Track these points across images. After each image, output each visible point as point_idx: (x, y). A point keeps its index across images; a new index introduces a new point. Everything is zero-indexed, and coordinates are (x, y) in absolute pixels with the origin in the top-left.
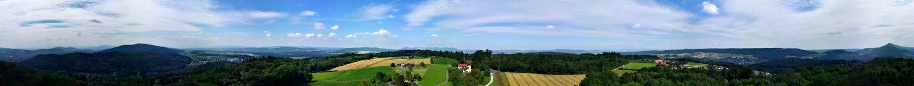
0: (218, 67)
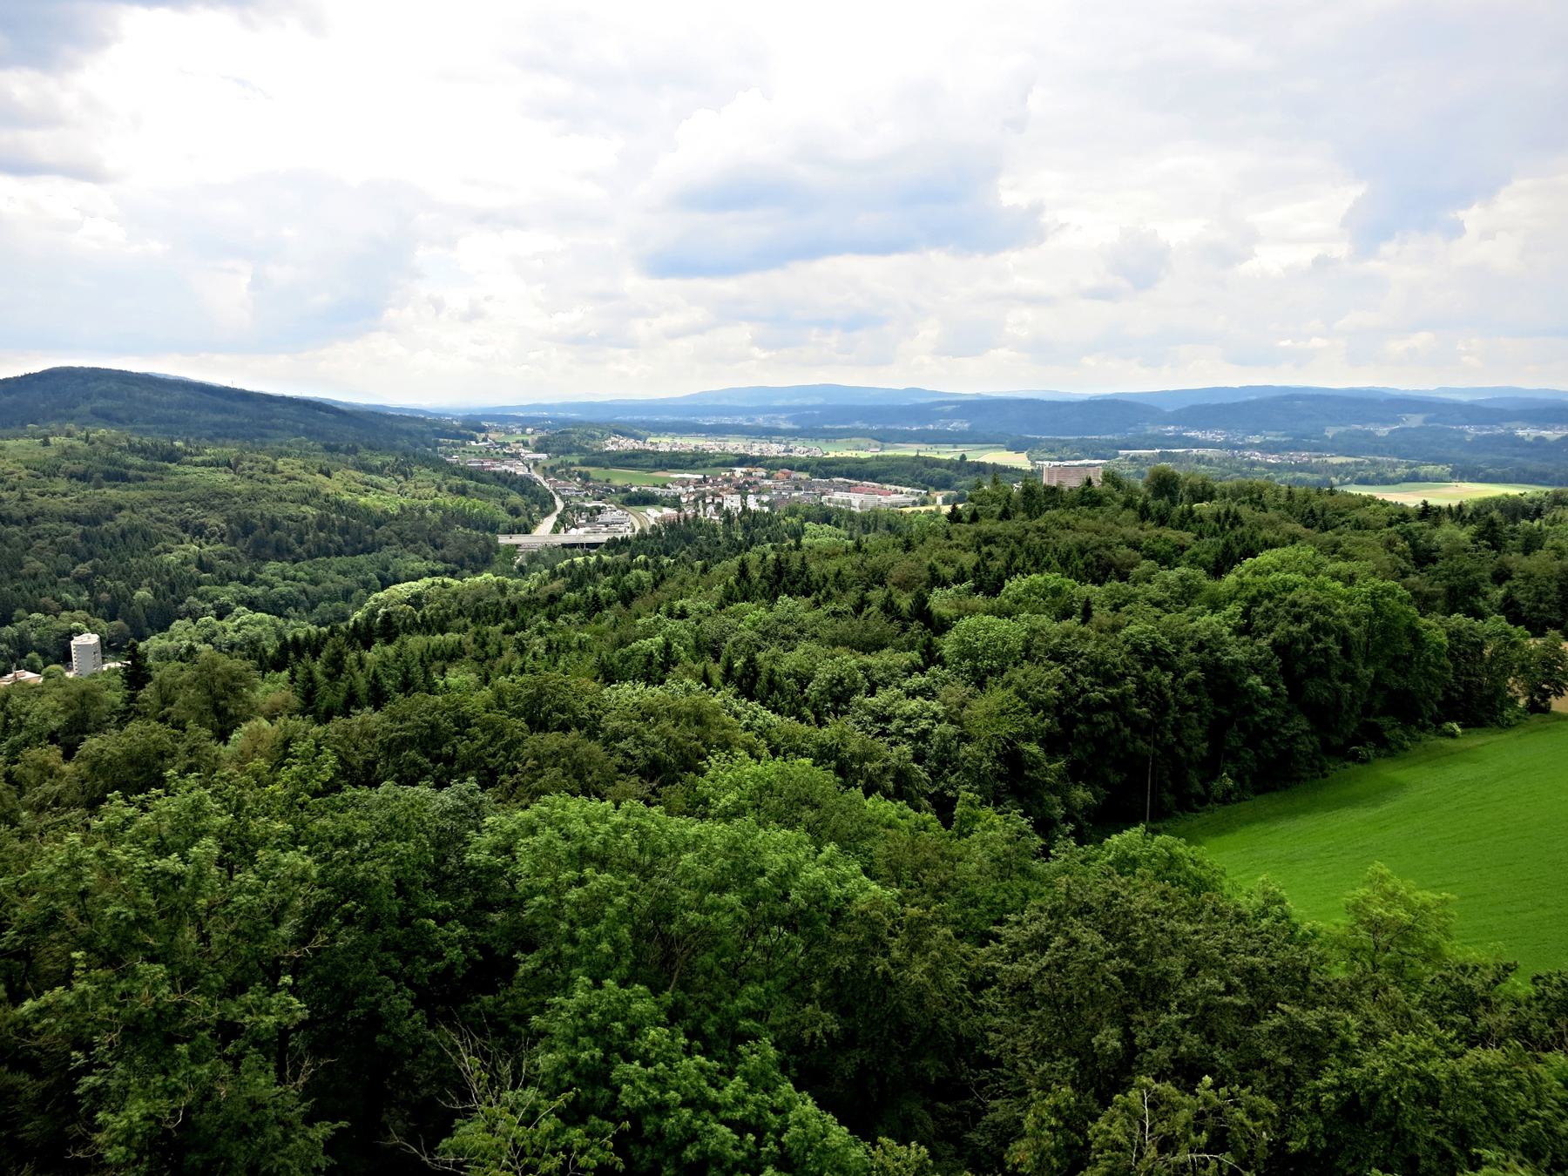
0: (753, 556)
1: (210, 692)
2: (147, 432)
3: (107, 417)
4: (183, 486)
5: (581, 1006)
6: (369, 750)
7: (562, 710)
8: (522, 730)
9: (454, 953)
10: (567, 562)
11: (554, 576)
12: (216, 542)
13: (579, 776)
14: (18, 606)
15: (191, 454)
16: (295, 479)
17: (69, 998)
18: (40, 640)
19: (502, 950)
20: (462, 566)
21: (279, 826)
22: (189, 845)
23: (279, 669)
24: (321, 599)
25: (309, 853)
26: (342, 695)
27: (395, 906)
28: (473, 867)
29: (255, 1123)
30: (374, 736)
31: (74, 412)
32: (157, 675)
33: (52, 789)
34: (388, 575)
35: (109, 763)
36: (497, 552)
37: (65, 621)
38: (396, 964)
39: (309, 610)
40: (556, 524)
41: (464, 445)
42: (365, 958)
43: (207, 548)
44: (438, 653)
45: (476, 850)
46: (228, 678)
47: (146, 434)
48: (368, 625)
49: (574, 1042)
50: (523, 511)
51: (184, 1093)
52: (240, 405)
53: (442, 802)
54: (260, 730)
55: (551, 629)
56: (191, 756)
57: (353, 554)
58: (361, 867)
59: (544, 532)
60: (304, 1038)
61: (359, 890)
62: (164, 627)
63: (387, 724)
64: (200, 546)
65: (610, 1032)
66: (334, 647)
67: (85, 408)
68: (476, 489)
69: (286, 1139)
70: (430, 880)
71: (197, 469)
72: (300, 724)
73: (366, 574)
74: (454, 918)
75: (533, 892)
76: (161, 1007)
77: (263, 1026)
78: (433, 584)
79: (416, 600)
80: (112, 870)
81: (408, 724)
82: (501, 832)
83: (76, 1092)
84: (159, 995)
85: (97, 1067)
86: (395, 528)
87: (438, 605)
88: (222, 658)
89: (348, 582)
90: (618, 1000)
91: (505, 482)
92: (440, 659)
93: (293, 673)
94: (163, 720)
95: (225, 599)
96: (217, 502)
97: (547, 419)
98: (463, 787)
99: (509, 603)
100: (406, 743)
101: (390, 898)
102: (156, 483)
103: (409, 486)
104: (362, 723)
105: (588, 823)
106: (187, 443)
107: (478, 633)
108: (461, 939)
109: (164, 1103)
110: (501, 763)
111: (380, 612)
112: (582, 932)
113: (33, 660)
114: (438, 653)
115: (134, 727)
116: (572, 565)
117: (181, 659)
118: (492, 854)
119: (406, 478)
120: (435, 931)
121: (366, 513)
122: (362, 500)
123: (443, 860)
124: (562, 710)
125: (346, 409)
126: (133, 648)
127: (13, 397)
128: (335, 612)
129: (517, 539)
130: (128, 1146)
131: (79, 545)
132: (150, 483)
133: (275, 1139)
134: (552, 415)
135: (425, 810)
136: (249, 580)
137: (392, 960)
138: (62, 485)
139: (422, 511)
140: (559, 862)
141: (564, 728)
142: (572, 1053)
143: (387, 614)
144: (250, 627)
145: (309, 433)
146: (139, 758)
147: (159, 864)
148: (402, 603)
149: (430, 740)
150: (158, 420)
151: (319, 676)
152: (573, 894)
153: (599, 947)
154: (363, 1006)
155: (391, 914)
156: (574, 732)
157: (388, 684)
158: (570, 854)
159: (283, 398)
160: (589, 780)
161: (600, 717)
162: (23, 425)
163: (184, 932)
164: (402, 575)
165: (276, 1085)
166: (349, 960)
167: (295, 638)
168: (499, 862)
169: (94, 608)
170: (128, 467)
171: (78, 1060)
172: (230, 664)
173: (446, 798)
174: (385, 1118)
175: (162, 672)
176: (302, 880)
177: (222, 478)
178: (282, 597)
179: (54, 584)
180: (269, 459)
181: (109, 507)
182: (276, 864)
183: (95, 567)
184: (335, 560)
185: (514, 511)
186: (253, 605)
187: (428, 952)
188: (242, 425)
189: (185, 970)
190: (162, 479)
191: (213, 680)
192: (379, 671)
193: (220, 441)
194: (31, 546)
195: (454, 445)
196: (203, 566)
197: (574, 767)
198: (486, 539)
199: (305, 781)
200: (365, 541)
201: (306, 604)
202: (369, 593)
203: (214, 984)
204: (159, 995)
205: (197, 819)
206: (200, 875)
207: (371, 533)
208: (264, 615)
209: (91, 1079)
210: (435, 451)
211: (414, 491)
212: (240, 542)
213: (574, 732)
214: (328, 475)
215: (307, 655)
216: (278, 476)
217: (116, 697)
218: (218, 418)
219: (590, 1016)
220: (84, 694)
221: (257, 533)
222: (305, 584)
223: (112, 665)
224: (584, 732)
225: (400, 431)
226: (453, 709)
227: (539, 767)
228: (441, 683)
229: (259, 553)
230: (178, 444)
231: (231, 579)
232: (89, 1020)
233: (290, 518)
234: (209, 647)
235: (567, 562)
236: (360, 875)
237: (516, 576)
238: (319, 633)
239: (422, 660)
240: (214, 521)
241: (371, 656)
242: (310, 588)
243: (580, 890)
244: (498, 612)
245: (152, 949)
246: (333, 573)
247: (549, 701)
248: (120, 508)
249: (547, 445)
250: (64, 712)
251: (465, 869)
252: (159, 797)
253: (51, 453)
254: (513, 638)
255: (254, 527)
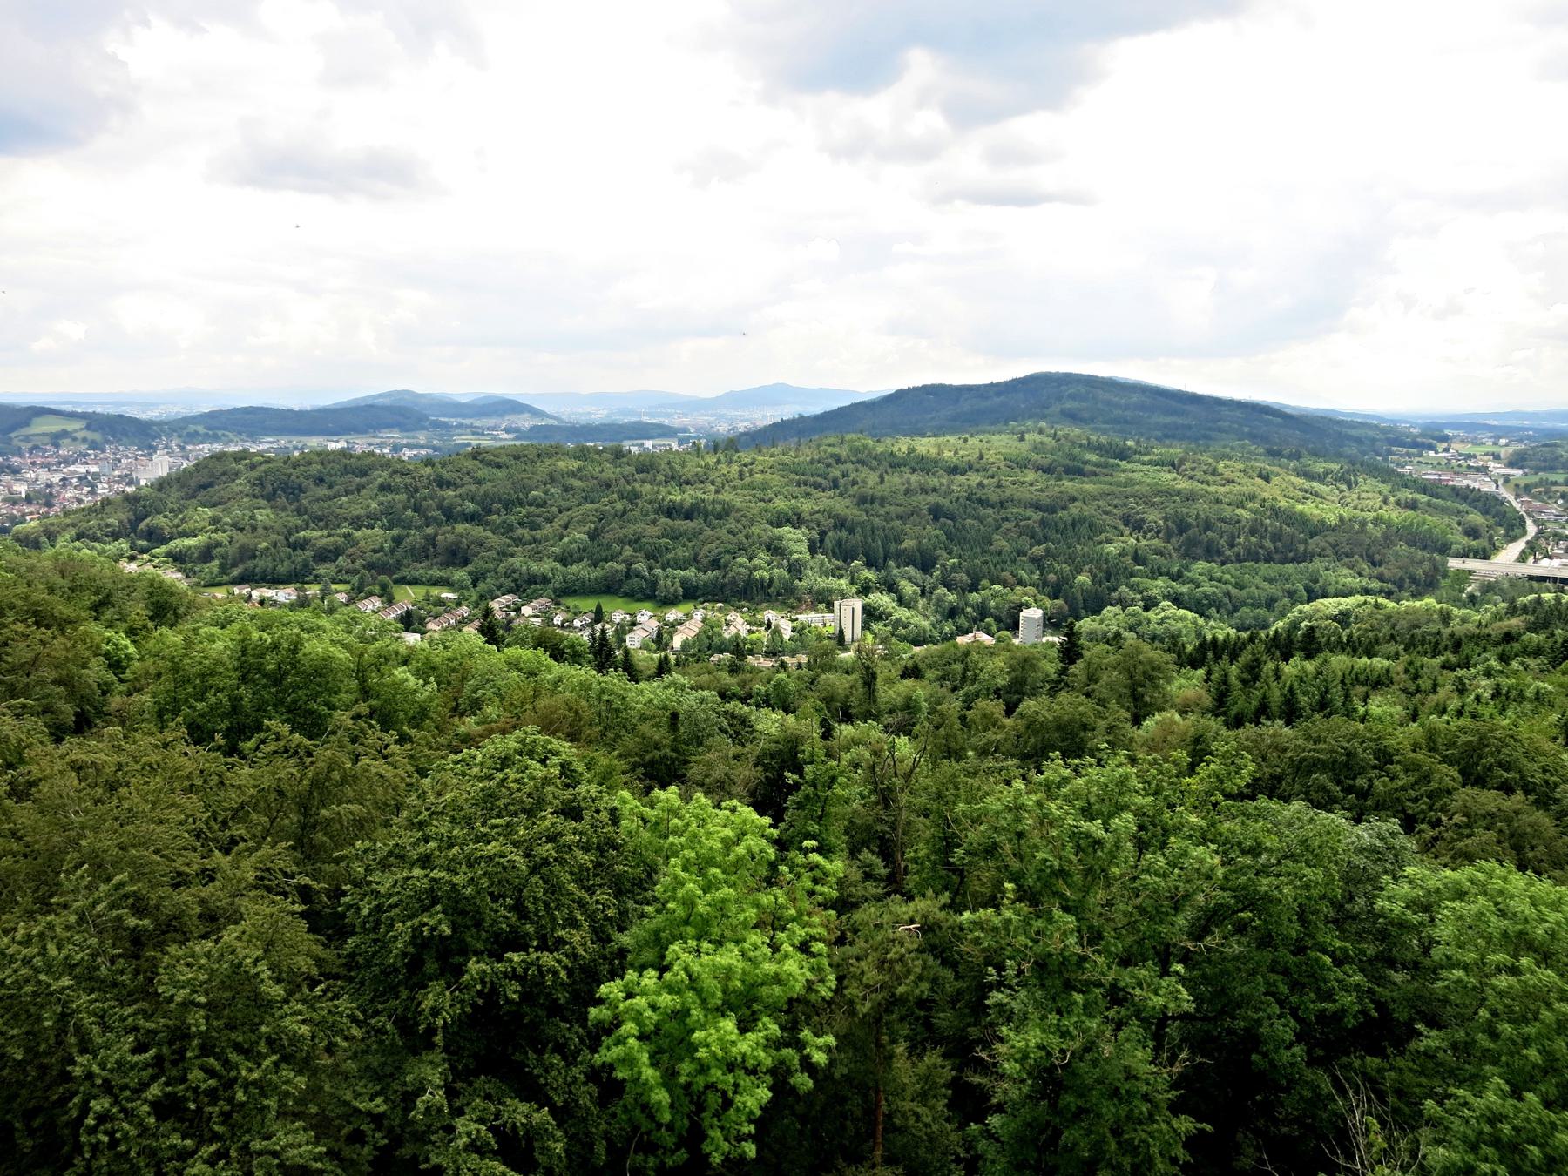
1: (1131, 677)
2: (1105, 432)
3: (1072, 417)
4: (1129, 483)
5: (1490, 1110)
6: (1278, 764)
7: (1507, 767)
8: (1453, 779)
9: (1348, 1000)
10: (1531, 597)
11: (1513, 611)
12: (1153, 538)
13: (1518, 848)
14: (984, 577)
15: (1140, 453)
16: (1233, 482)
17: (997, 921)
18: (997, 608)
19: (1401, 1014)
20: (1401, 588)
21: (1193, 818)
22: (1111, 816)
23: (1195, 667)
24: (1244, 604)
25: (1217, 852)
26: (1255, 703)
27: (1294, 930)
28: (1382, 915)
29: (1127, 1091)
30: (1285, 750)
31: (1046, 412)
32: (1087, 654)
33: (994, 737)
34: (1317, 588)
35: (1042, 724)
36: (1445, 576)
37: (1019, 594)
38: (1284, 989)
39: (1231, 613)
40: (1523, 552)
41: (1420, 455)
42: (1253, 973)
43: (1144, 542)
44: (1362, 678)
45: (1389, 899)
46: (1148, 668)
47: (1104, 434)
48: (1289, 636)
49: (1474, 1148)
50: (1484, 534)
51: (1073, 1038)
52: (1189, 408)
53: (1358, 837)
54: (1173, 722)
55: (1501, 672)
56: (1109, 733)
57: (1283, 562)
58: (1266, 881)
59: (1507, 560)
60: (1180, 1028)
61: (1251, 900)
62: (1097, 611)
63: (1300, 742)
64: (1138, 540)
65: (1523, 1154)
66: (1253, 654)
67: (1056, 408)
68: (1429, 504)
69: (1151, 1119)
70: (1331, 914)
71: (1144, 468)
72: (1214, 724)
73: (1294, 584)
74: (1351, 963)
75: (1451, 963)
76: (1067, 954)
77: (1150, 1004)
78: (1365, 603)
79: (1343, 618)
80: (1045, 820)
81: (1322, 746)
82: (1422, 887)
83: (987, 1002)
84: (1067, 942)
85: (1005, 986)
86: (1331, 540)
87: (1367, 626)
88: (1146, 647)
89: (1273, 590)
90: (1540, 1121)
91: (1465, 499)
92: (1363, 684)
93: (1209, 673)
94: (1088, 695)
95: (1154, 592)
96: (1157, 499)
97: (1527, 429)
98: (1385, 826)
99: (1452, 635)
100: (1316, 765)
101: (1290, 920)
102: (1108, 479)
103: (1352, 497)
104: (1274, 736)
105: (1534, 904)
106: (1138, 442)
107: (1411, 663)
108: (1357, 987)
109: (1056, 1040)
110: (1422, 811)
111: (1303, 625)
112: (1506, 1028)
113: (989, 625)
114: (1362, 678)
115: (1063, 697)
116: (1539, 601)
117: (1108, 643)
118: (1407, 907)
119: (1350, 488)
120: (1329, 969)
121: (1302, 521)
122: (1300, 507)
123: (1351, 898)
124: (1507, 767)
125: (1294, 413)
126: (1071, 626)
127: (1002, 398)
128: (1256, 618)
129: (1471, 564)
130: (1022, 1065)
131: (1038, 530)
132: (1102, 479)
133: (1141, 1113)
134: (1536, 424)
135: (1339, 841)
136: (1177, 577)
137: (1280, 984)
138: (1030, 476)
139: (1363, 524)
140: (1489, 940)
141: (1507, 789)
142: (1470, 1158)
143: (1312, 629)
144: (1173, 622)
145: (1253, 437)
146: (1066, 726)
147: (1085, 826)
148: (1327, 618)
149: (1345, 768)
150: (1116, 421)
151: (1233, 680)
152: (1503, 981)
153: (1525, 1052)
154: (1244, 1019)
155: (1286, 938)
156: (1519, 796)
157: (1304, 701)
158: (1505, 934)
159: (1232, 401)
160: (1530, 855)
161: (1556, 785)
162: (1006, 423)
163: (1097, 893)
164: (1331, 589)
165: (1151, 1063)
166: (1239, 970)
167: (1215, 639)
168: (1414, 918)
169: (1042, 585)
170: (1086, 463)
171: (991, 975)
172: (1152, 654)
173: (1364, 834)
174: (1240, 1137)
175: (1093, 652)
176: (1208, 878)
177: (1167, 477)
178: (1206, 596)
179: (1014, 561)
180: (1210, 461)
181: (1066, 498)
182: (1185, 854)
183: (1047, 550)
184: (1263, 566)
185: (1472, 532)
186: (1177, 601)
187: (1319, 989)
188: (1189, 427)
189: (1091, 928)
190: (1111, 475)
191: (1135, 666)
192: (1296, 686)
193: (1167, 442)
194: (1000, 527)
195: (1408, 455)
196: (1138, 559)
197: (1512, 836)
198: (1432, 560)
199: (1221, 782)
200: (1297, 550)
201: (1227, 607)
202: (1294, 604)
203: (1113, 949)
204: (1067, 942)
205: (1120, 794)
206: (1117, 845)
207: (1305, 542)
208: (1187, 612)
209: (1000, 996)
210: (1386, 460)
211: (1356, 502)
212: (1174, 540)
213: (1519, 796)
214: (1267, 479)
215: (1225, 657)
216: (1218, 478)
217: (1050, 668)
218: (1168, 420)
219: (1500, 1125)
220: (1026, 660)
221: (1191, 531)
222: (1230, 587)
223: (1051, 639)
224: (1532, 798)
225: (1350, 438)
226: (1375, 740)
227: (1468, 826)
228: (1362, 710)
229: (1189, 554)
230: (1130, 443)
231: (1161, 574)
232: (1009, 945)
233: (1223, 520)
234: (1133, 635)
235: (1531, 597)
236: (1264, 888)
237: (1465, 606)
238: (1238, 638)
239: (1343, 682)
240: (1154, 517)
241: (1290, 669)
242: (1234, 591)
243: (1512, 980)
244: (1437, 643)
245: (1067, 900)
246: (1259, 579)
247: (1492, 754)
248: (1074, 499)
249: (1523, 459)
250: (1008, 673)
251: (1374, 915)
252: (1091, 765)
253: (1024, 447)
254: (1452, 675)
255: (1189, 526)
